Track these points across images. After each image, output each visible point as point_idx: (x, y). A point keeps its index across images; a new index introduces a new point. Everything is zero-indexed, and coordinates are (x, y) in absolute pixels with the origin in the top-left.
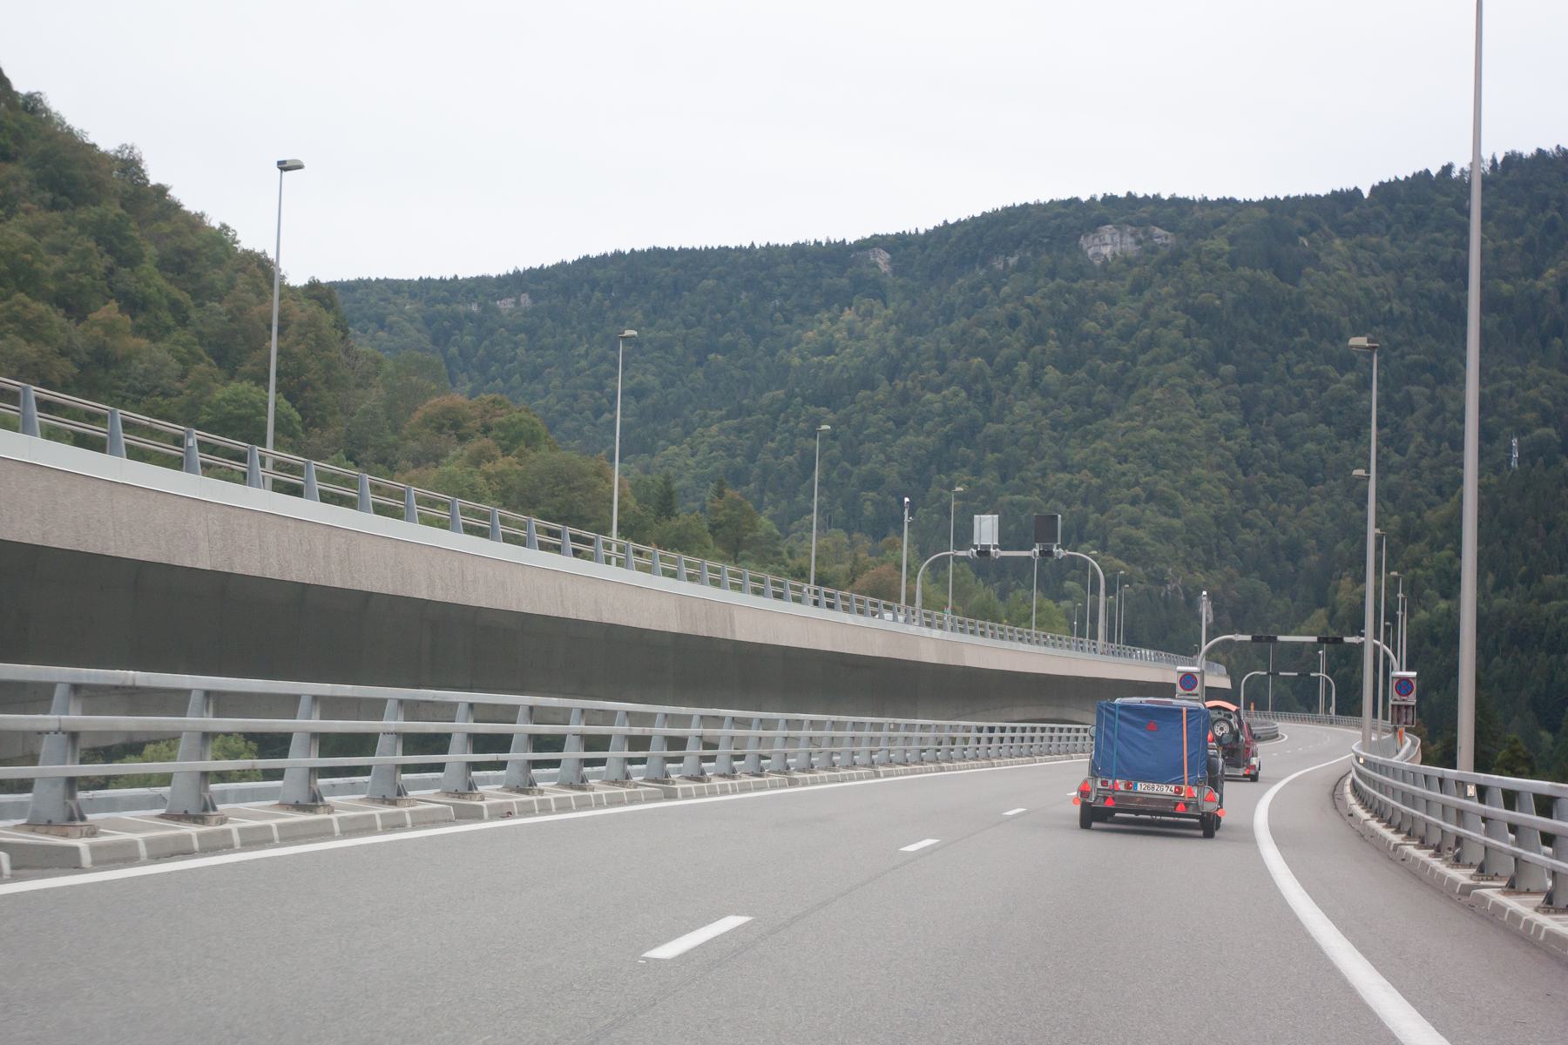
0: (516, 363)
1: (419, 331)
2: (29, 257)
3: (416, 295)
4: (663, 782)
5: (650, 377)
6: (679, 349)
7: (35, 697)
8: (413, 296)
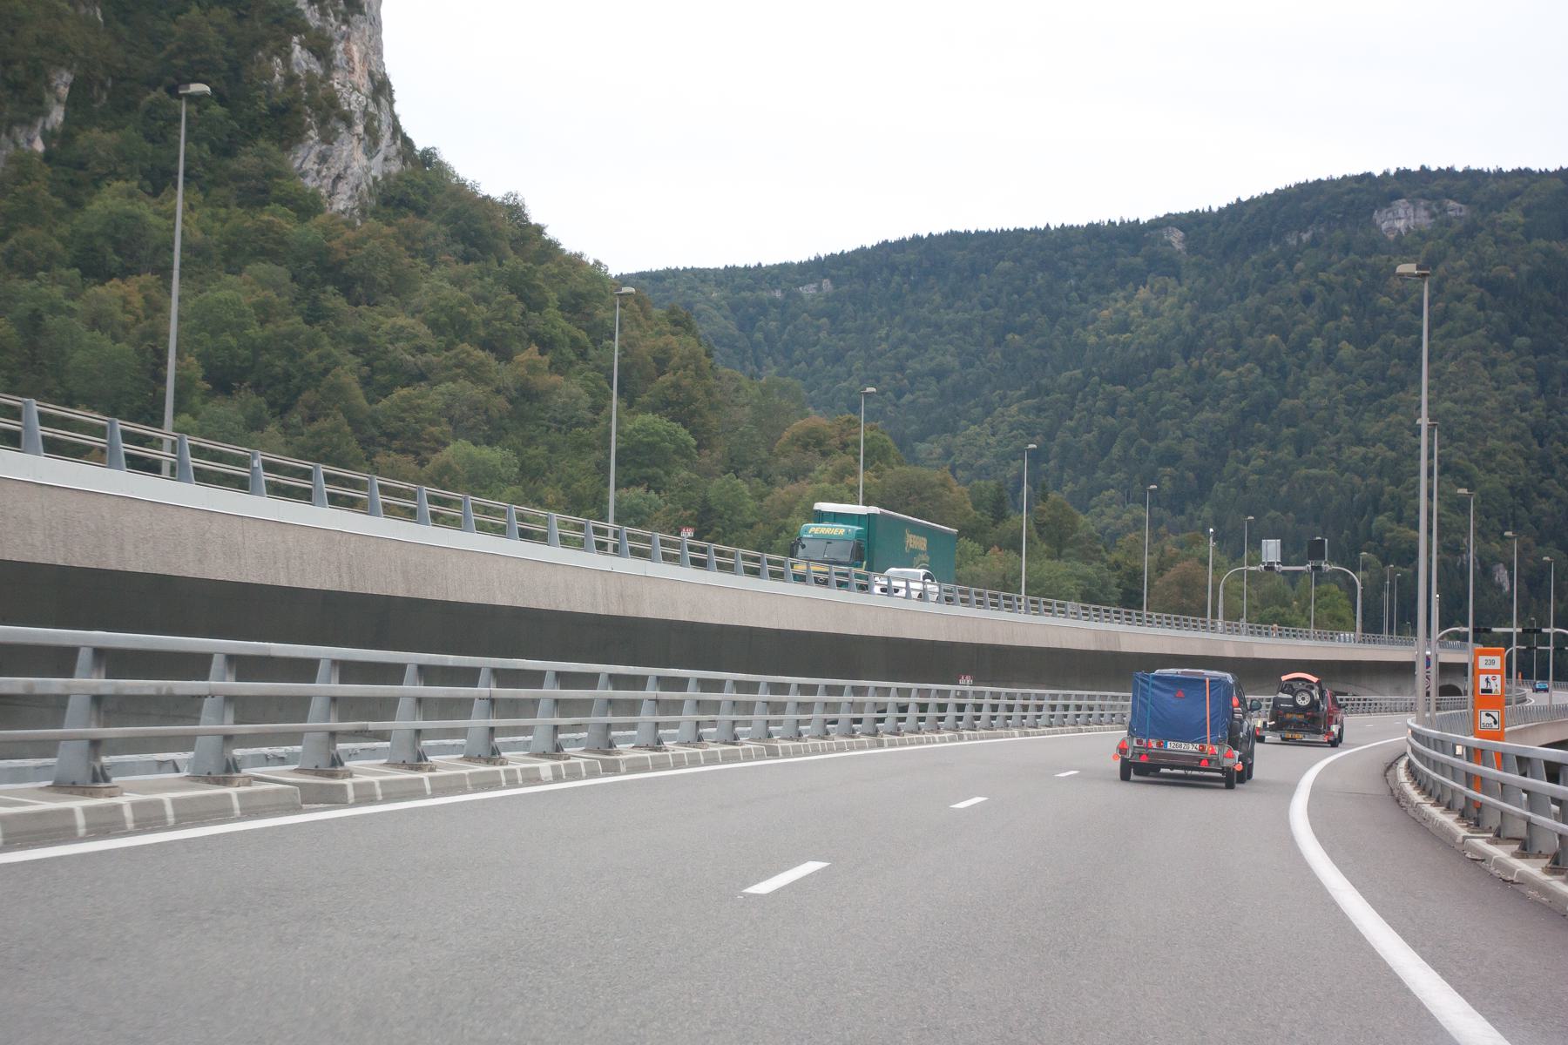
0: (818, 347)
1: (726, 318)
2: (464, 310)
3: (722, 283)
5: (949, 358)
6: (977, 330)
8: (719, 284)
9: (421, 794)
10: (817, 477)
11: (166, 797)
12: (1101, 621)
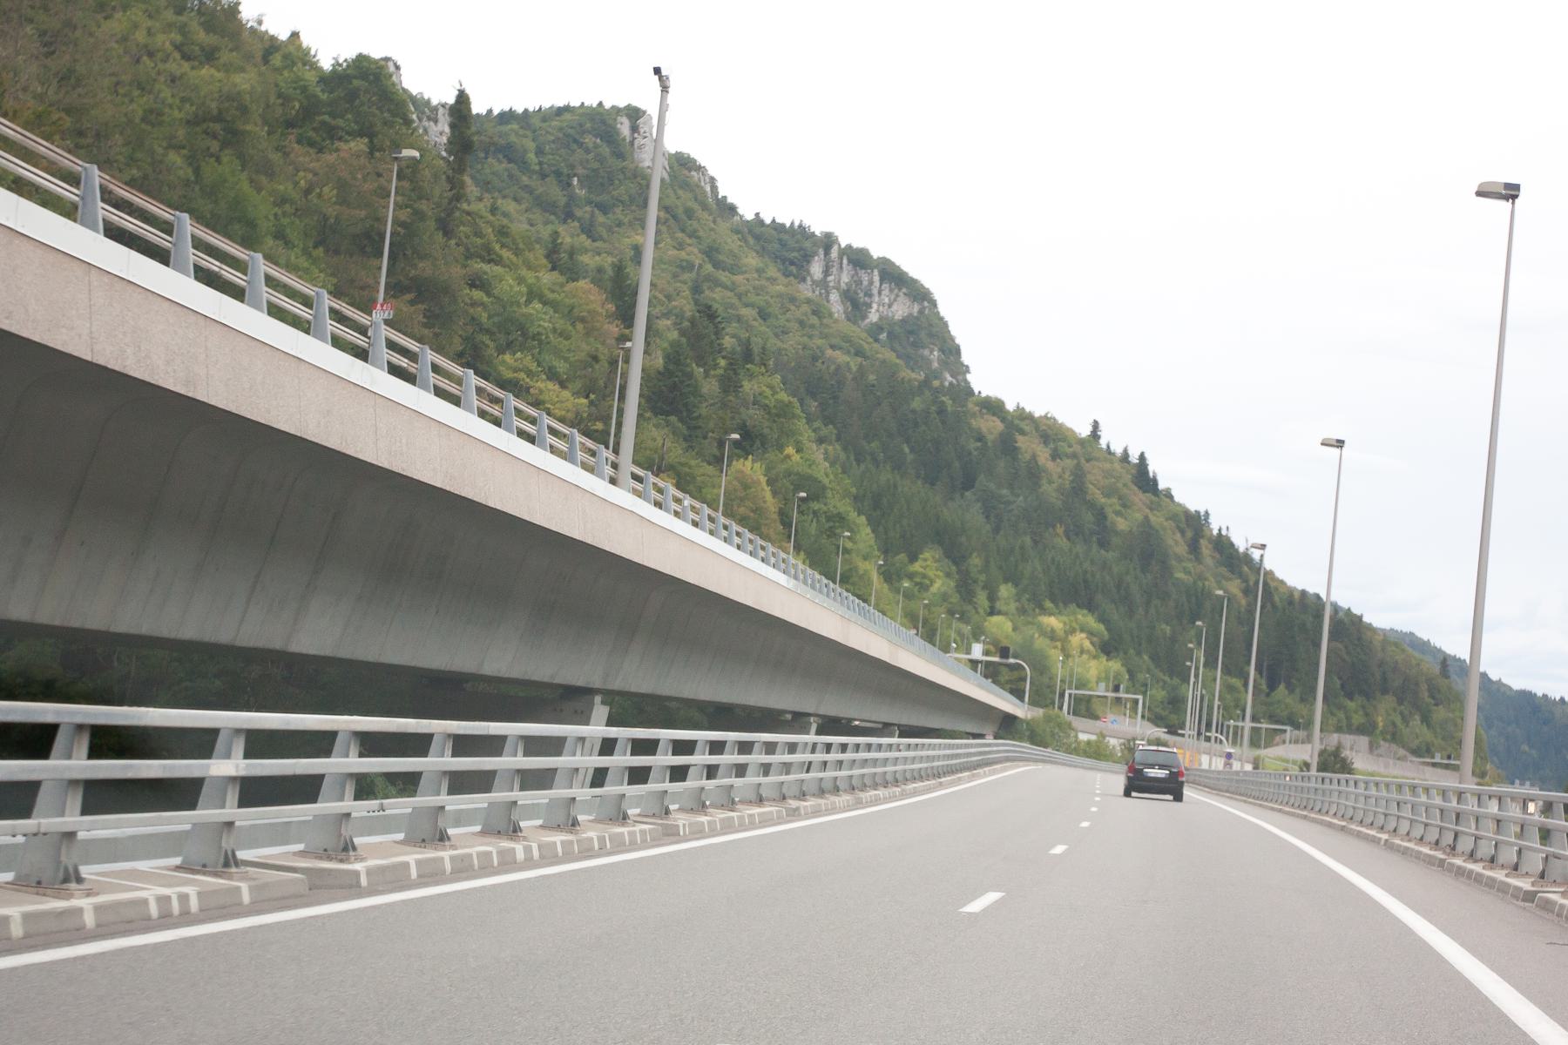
7: (37, 740)
9: (81, 935)
10: (975, 582)
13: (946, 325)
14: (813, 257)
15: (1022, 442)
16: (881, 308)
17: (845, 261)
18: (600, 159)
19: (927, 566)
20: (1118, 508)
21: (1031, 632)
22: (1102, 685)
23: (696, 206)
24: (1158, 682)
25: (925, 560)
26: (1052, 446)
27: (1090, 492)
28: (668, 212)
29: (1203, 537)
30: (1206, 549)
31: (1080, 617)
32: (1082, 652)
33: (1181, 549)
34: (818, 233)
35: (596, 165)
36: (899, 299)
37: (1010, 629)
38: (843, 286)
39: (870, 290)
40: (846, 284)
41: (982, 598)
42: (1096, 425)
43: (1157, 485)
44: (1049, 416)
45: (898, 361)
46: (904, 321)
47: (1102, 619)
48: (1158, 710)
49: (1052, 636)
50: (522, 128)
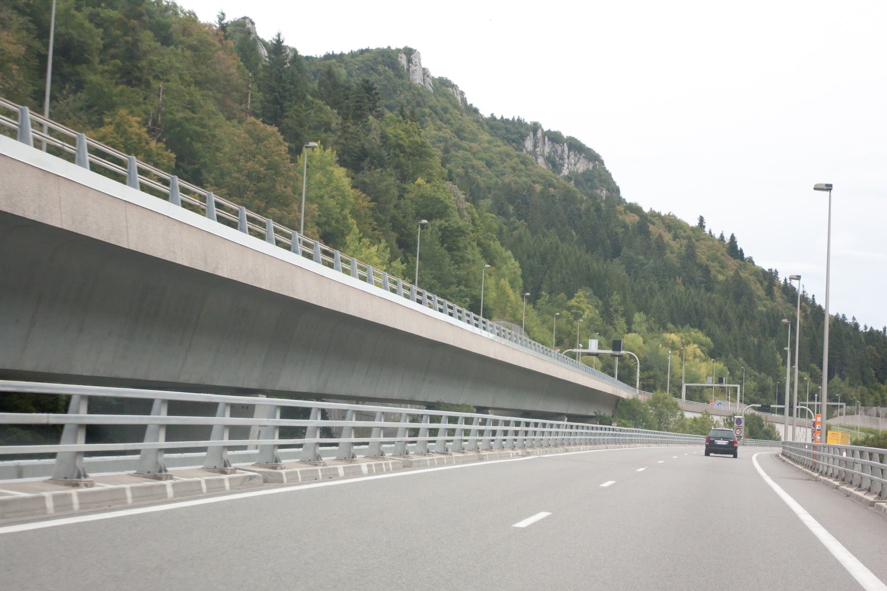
4: (445, 454)
11: (298, 470)
12: (567, 363)
13: (610, 175)
14: (526, 137)
15: (651, 228)
16: (570, 167)
17: (546, 139)
18: (388, 79)
19: (581, 301)
20: (718, 268)
21: (656, 344)
22: (710, 379)
23: (449, 106)
24: (750, 376)
25: (579, 297)
26: (673, 232)
27: (699, 257)
28: (432, 109)
29: (775, 285)
30: (777, 293)
31: (693, 333)
32: (695, 357)
33: (761, 292)
34: (529, 123)
35: (386, 82)
36: (580, 160)
37: (642, 342)
38: (546, 154)
39: (563, 156)
40: (548, 153)
41: (621, 322)
42: (701, 219)
43: (743, 254)
44: (671, 214)
45: (576, 189)
46: (584, 174)
47: (709, 334)
48: (752, 396)
49: (673, 347)
50: (338, 62)
